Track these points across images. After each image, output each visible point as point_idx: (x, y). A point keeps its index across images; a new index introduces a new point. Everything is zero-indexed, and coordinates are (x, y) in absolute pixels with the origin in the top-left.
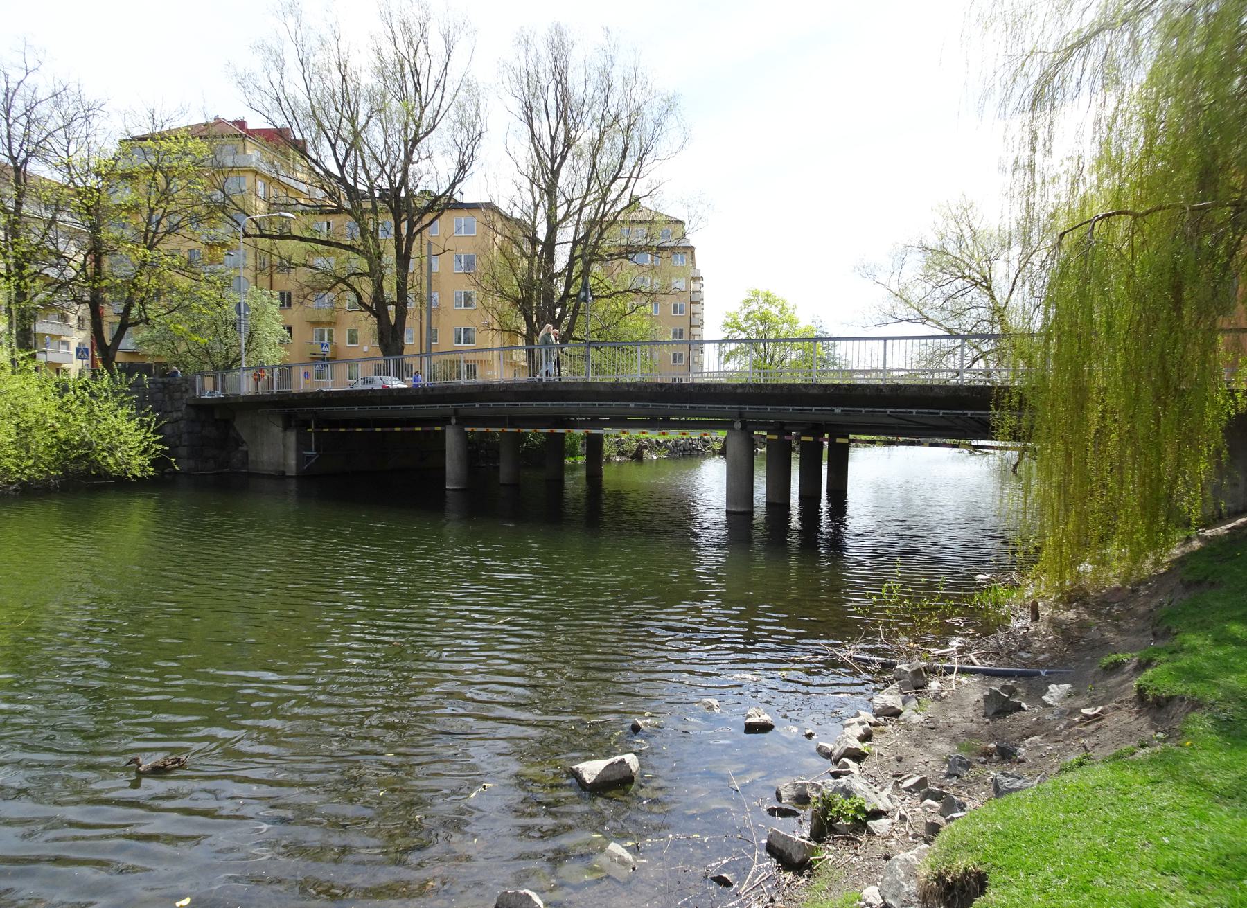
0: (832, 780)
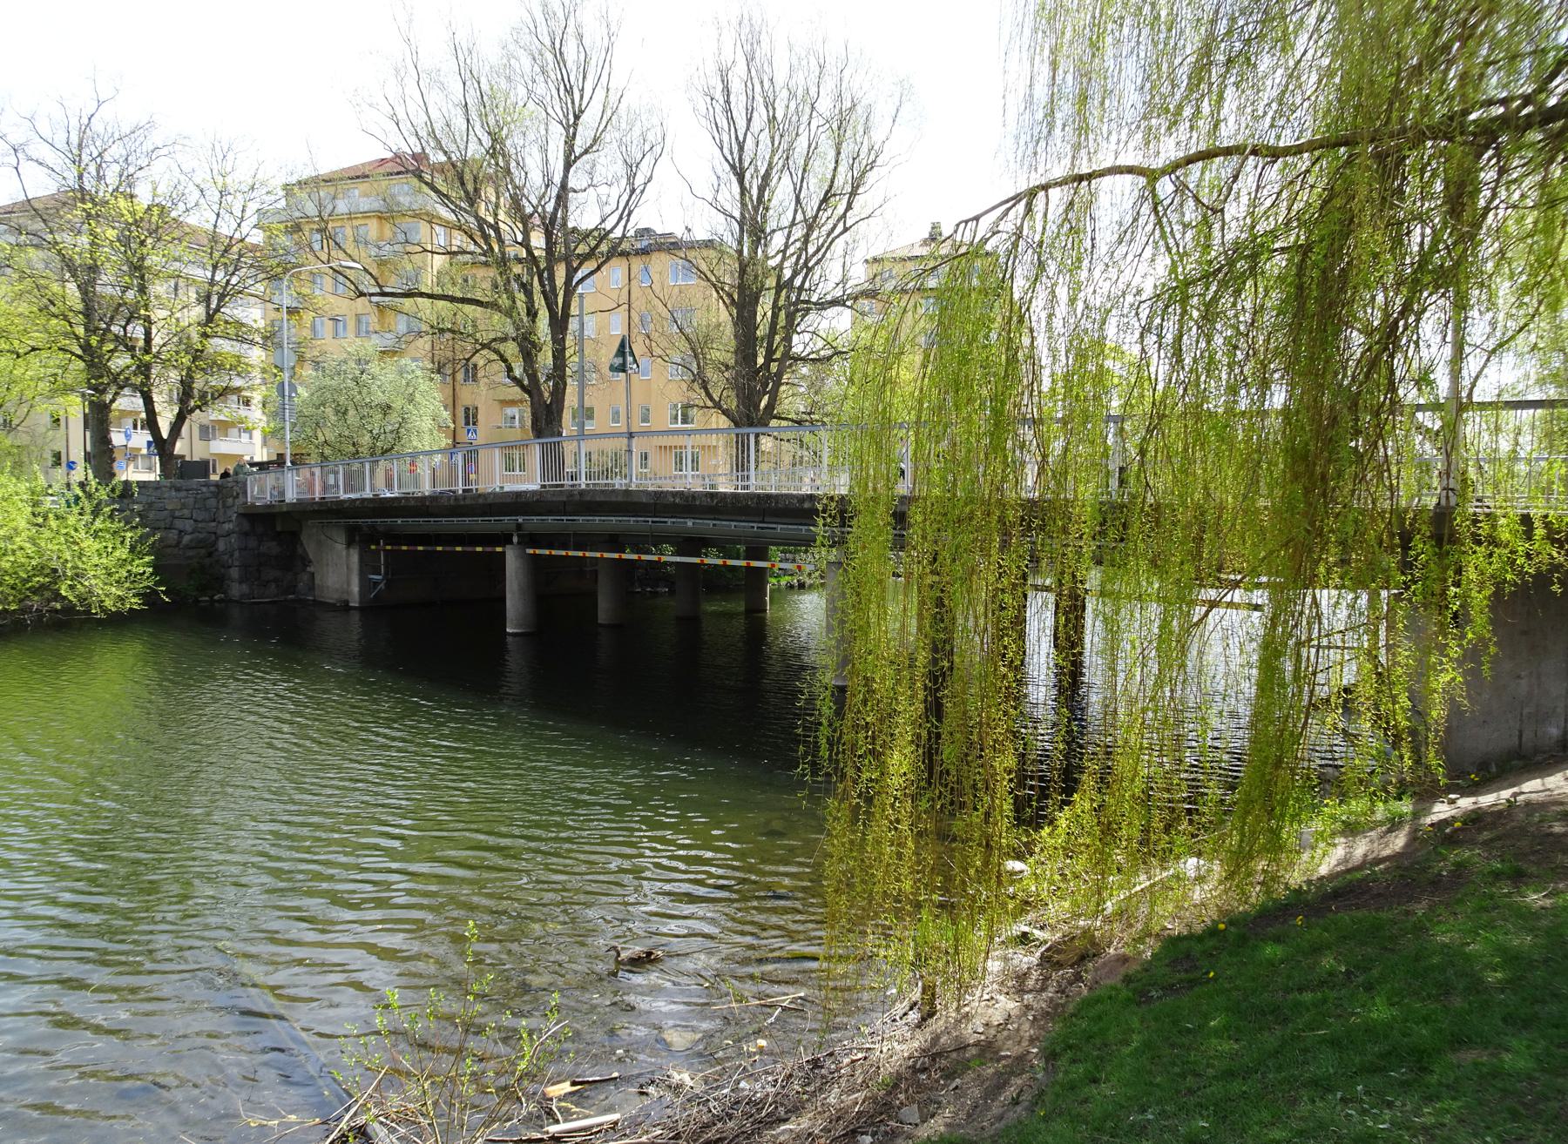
0: (1019, 1109)
